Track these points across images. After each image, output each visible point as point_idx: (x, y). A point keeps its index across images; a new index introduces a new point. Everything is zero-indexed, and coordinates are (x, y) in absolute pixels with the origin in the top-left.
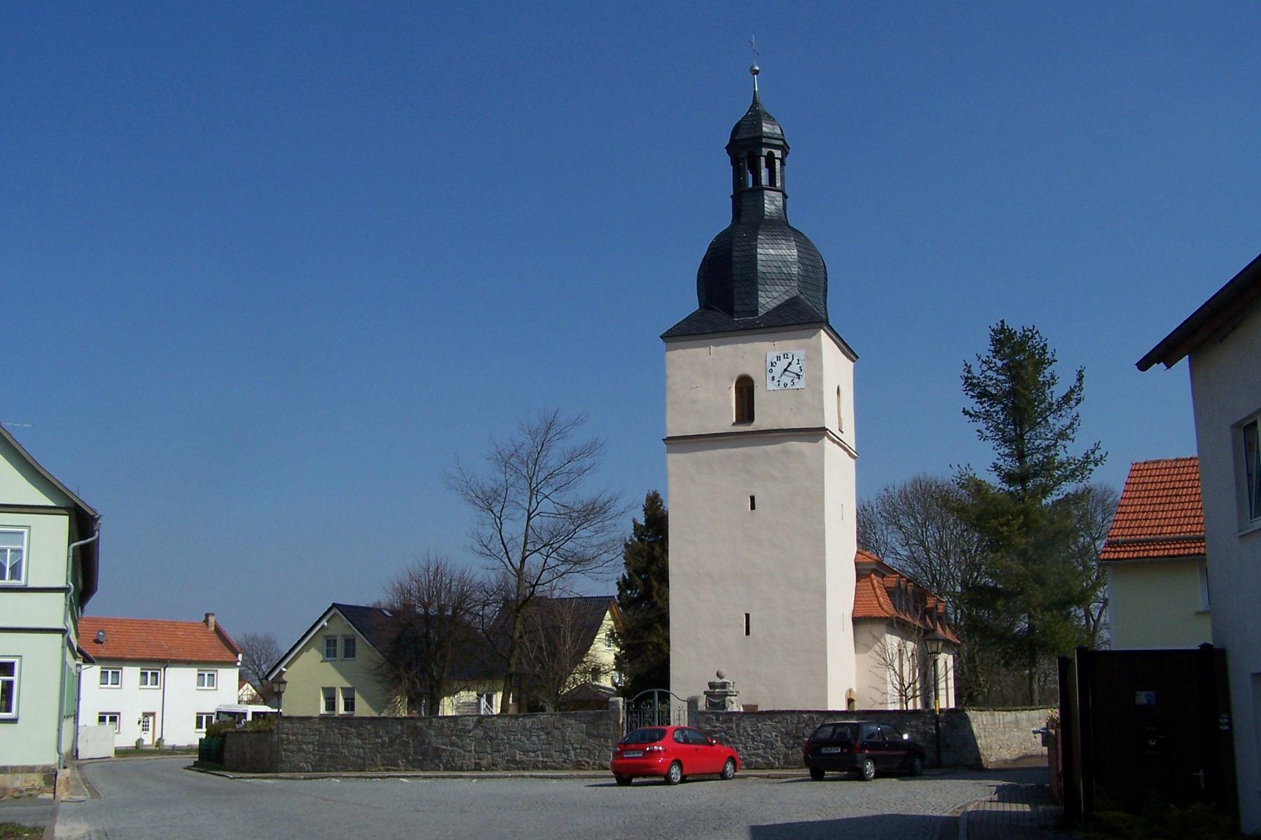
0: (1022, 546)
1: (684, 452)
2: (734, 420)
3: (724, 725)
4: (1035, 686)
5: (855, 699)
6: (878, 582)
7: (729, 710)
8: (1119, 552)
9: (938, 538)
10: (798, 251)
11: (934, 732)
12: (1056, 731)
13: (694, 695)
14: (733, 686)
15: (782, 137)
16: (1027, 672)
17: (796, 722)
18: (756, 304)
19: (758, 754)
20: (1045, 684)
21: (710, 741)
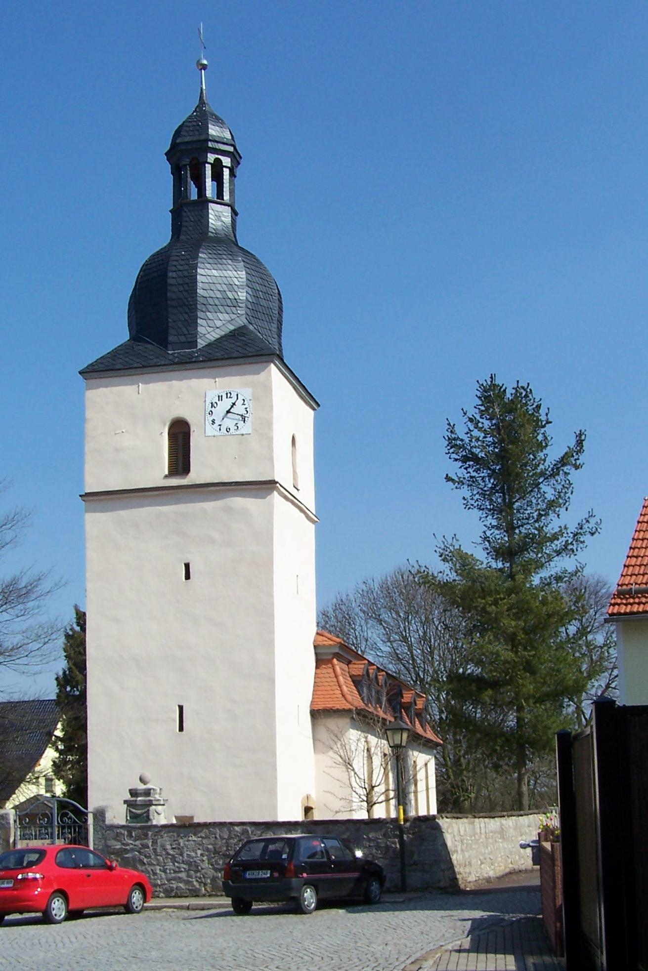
0: (511, 629)
1: (102, 512)
2: (167, 473)
3: (138, 843)
4: (525, 788)
5: (313, 807)
6: (341, 669)
7: (154, 823)
8: (631, 604)
9: (421, 634)
10: (247, 273)
11: (398, 846)
12: (552, 846)
13: (100, 805)
14: (160, 794)
15: (233, 143)
16: (516, 775)
17: (226, 837)
18: (195, 335)
19: (180, 878)
20: (535, 788)
21: (109, 863)
